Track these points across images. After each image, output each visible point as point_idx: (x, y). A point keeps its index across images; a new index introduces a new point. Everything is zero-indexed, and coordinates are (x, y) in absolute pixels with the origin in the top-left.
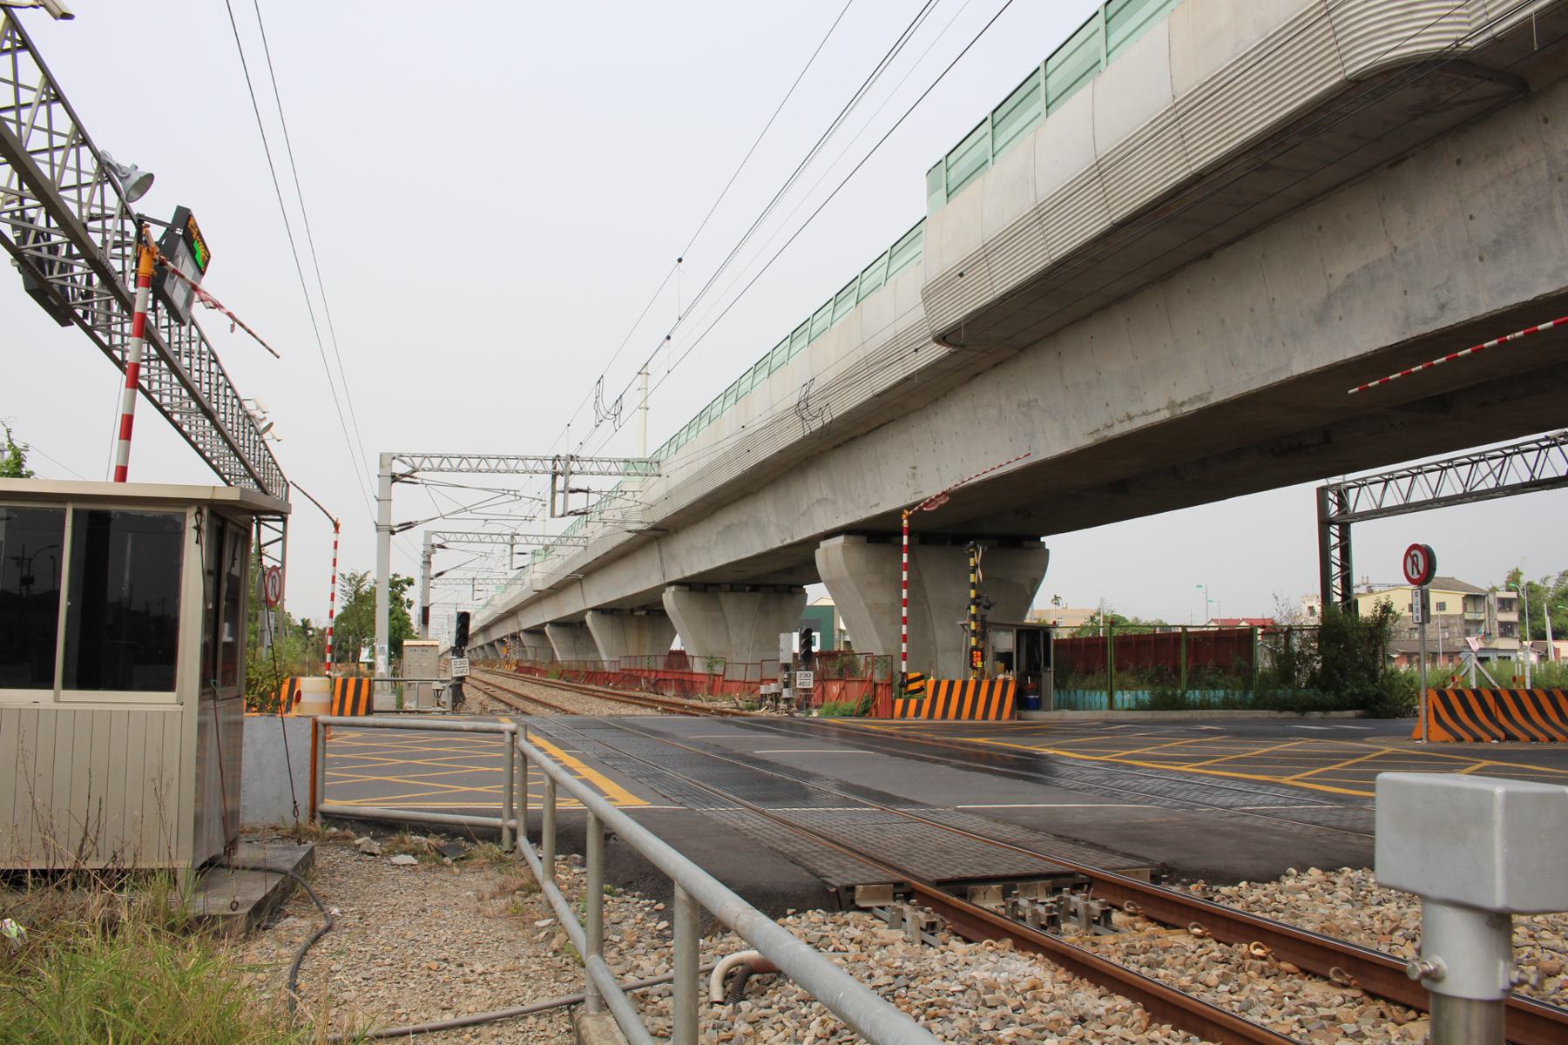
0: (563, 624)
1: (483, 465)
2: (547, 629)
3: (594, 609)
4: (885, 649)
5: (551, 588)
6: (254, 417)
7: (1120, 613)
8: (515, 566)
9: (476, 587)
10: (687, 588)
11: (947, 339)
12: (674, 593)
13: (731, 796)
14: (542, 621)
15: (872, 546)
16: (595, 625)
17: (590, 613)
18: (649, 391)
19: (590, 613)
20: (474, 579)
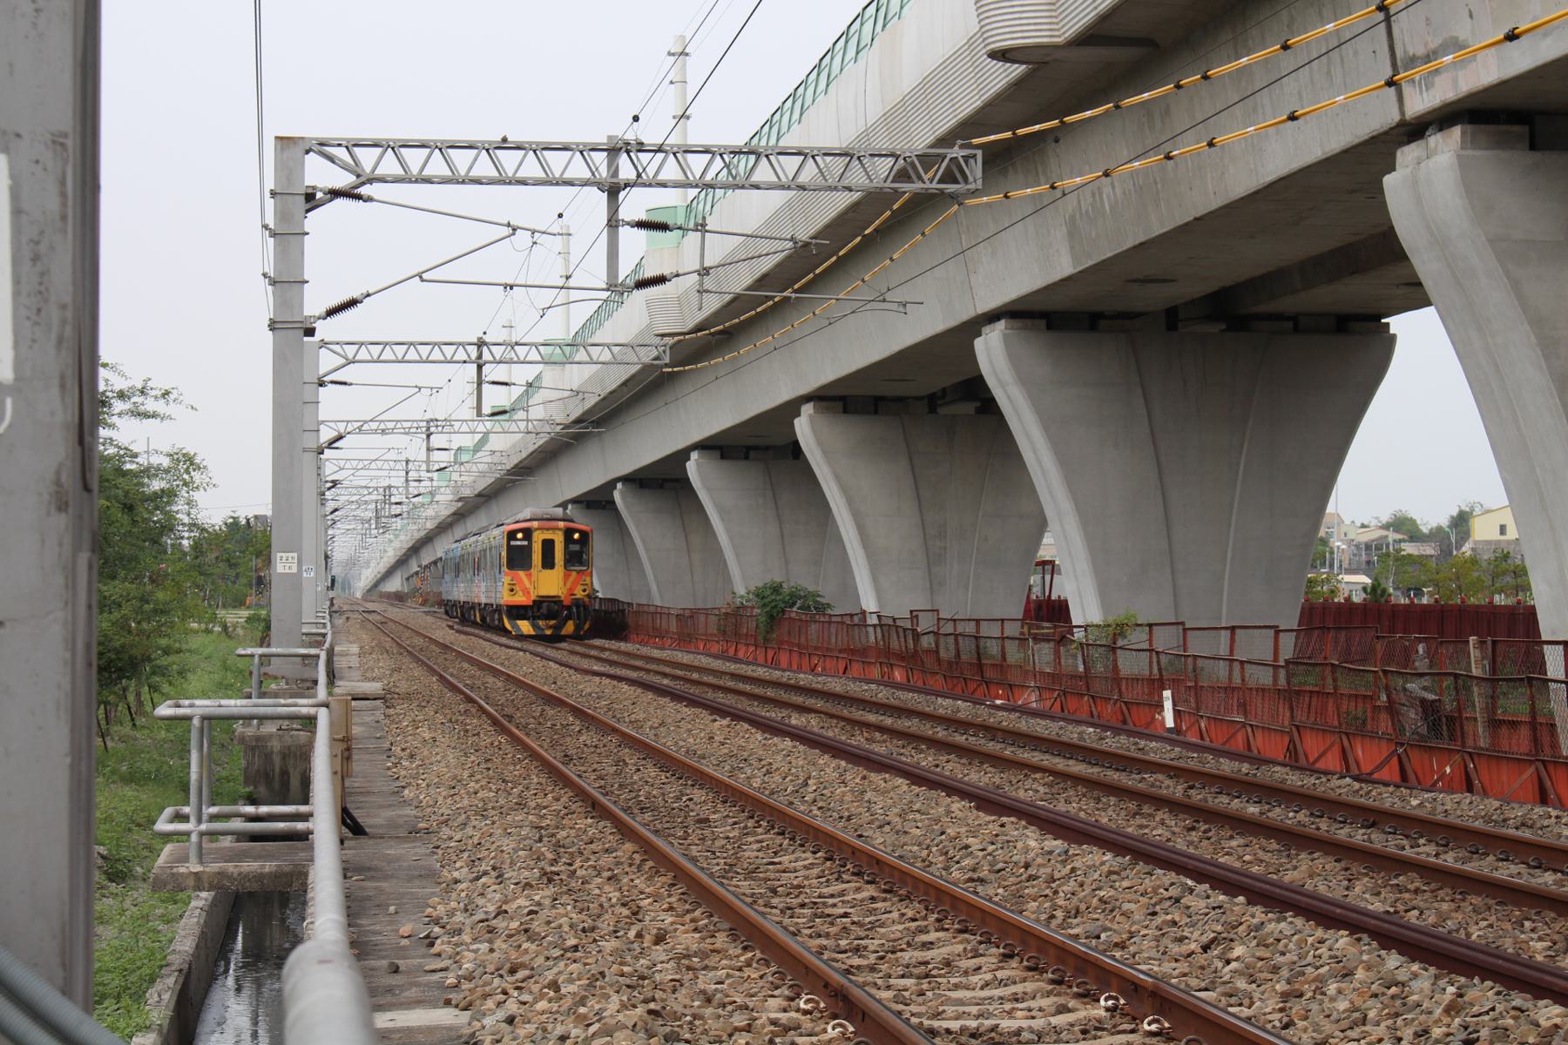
0: (641, 481)
1: (412, 355)
2: (804, 427)
3: (1018, 313)
4: (1105, 605)
5: (479, 495)
6: (226, 978)
7: (1413, 514)
8: (486, 410)
9: (491, 373)
10: (1043, 323)
11: (1007, 56)
12: (1006, 339)
13: (282, 701)
14: (784, 394)
15: (725, 463)
16: (1023, 380)
17: (807, 409)
18: (574, 260)
19: (807, 409)
20: (407, 462)
